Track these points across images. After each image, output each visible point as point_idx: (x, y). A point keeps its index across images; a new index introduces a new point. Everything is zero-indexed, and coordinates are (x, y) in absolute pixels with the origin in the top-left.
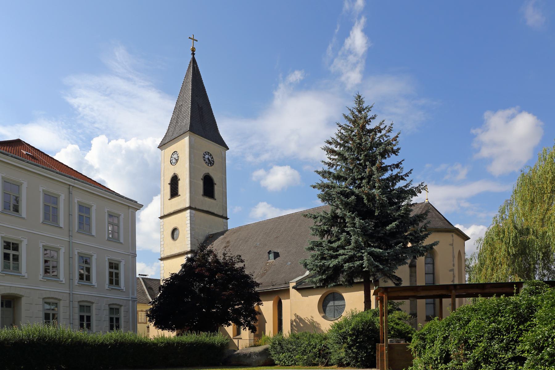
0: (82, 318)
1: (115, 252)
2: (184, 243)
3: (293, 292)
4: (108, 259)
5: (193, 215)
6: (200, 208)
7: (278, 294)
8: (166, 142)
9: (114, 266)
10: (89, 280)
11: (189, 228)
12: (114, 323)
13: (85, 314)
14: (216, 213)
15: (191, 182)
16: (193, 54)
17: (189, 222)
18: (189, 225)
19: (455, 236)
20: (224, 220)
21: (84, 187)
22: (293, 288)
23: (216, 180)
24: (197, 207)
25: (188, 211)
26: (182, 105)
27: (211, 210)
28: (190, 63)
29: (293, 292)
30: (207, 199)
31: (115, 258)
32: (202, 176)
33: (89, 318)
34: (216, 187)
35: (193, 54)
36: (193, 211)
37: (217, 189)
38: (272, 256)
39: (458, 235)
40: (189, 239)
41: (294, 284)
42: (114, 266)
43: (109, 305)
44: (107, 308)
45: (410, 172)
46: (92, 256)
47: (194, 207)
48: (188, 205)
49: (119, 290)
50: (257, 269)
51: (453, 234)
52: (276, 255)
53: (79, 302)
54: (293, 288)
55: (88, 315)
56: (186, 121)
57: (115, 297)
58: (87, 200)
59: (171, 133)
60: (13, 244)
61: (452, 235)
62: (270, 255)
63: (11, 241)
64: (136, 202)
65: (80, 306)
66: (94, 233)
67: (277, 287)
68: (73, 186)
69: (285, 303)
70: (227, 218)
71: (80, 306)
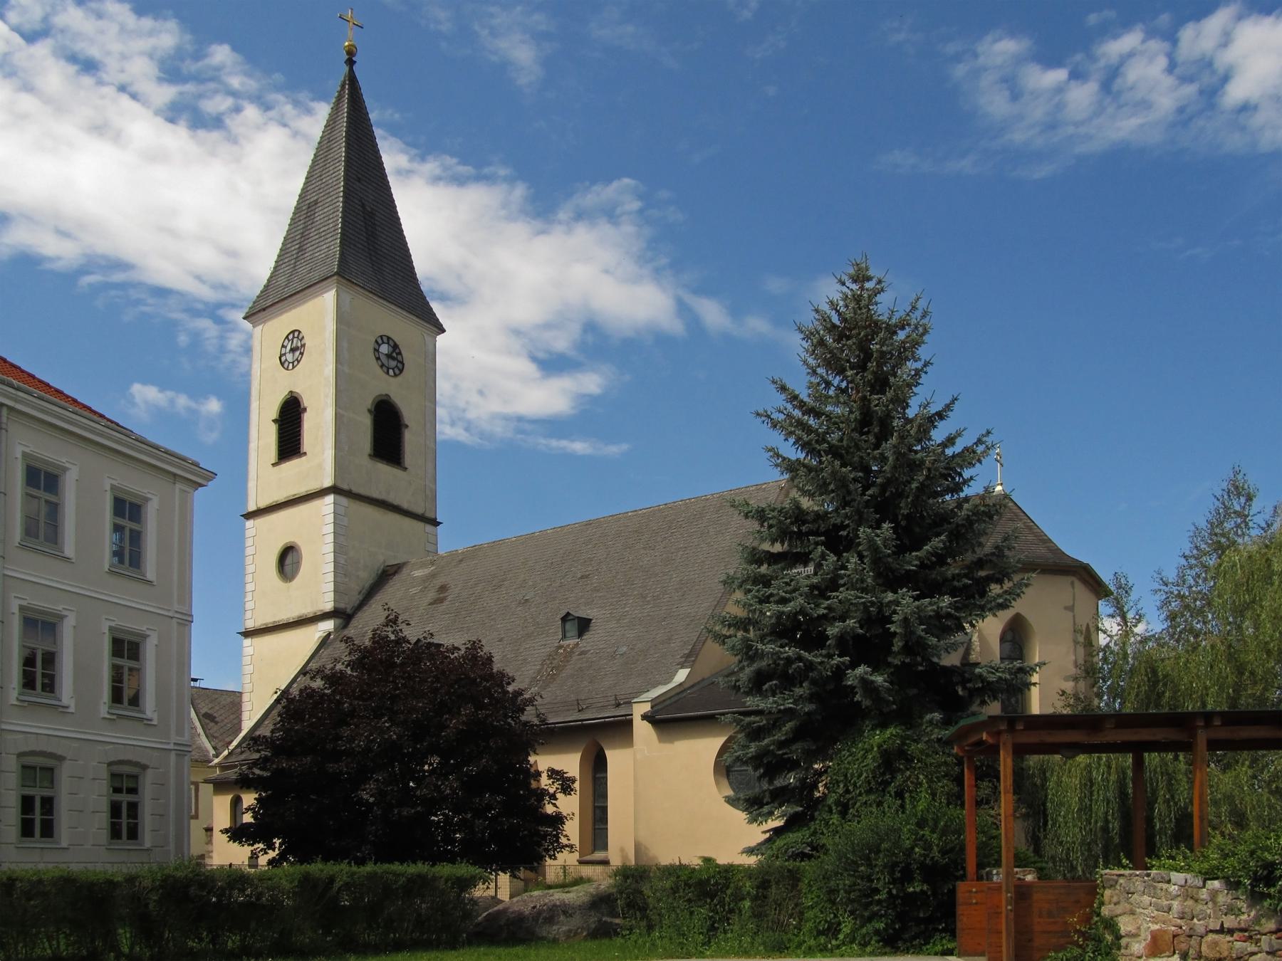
0: (27, 803)
1: (127, 605)
2: (317, 587)
3: (642, 729)
4: (111, 629)
5: (342, 511)
6: (362, 491)
7: (598, 735)
8: (269, 302)
9: (126, 648)
10: (52, 691)
11: (330, 548)
12: (124, 821)
13: (38, 793)
14: (405, 506)
15: (338, 417)
16: (350, 62)
17: (331, 528)
18: (331, 538)
19: (1079, 587)
20: (429, 528)
21: (42, 411)
22: (645, 717)
23: (408, 413)
24: (355, 490)
25: (330, 499)
26: (316, 202)
27: (392, 498)
28: (343, 86)
29: (642, 729)
30: (384, 469)
31: (132, 624)
32: (369, 403)
33: (48, 804)
34: (408, 436)
35: (350, 62)
36: (344, 501)
37: (410, 440)
38: (572, 628)
39: (1085, 582)
40: (331, 577)
41: (647, 708)
42: (126, 648)
43: (110, 764)
44: (104, 773)
45: (948, 407)
46: (62, 617)
47: (345, 487)
48: (328, 482)
49: (142, 719)
50: (523, 659)
51: (1074, 579)
52: (584, 625)
53: (20, 755)
54: (645, 717)
55: (46, 793)
56: (329, 248)
57: (126, 740)
58: (51, 451)
59: (282, 280)
60: (131, 504)
61: (1072, 583)
62: (568, 625)
63: (127, 637)
64: (197, 465)
65: (24, 767)
66: (69, 551)
67: (591, 716)
68: (11, 409)
69: (616, 758)
70: (435, 523)
71: (24, 767)
